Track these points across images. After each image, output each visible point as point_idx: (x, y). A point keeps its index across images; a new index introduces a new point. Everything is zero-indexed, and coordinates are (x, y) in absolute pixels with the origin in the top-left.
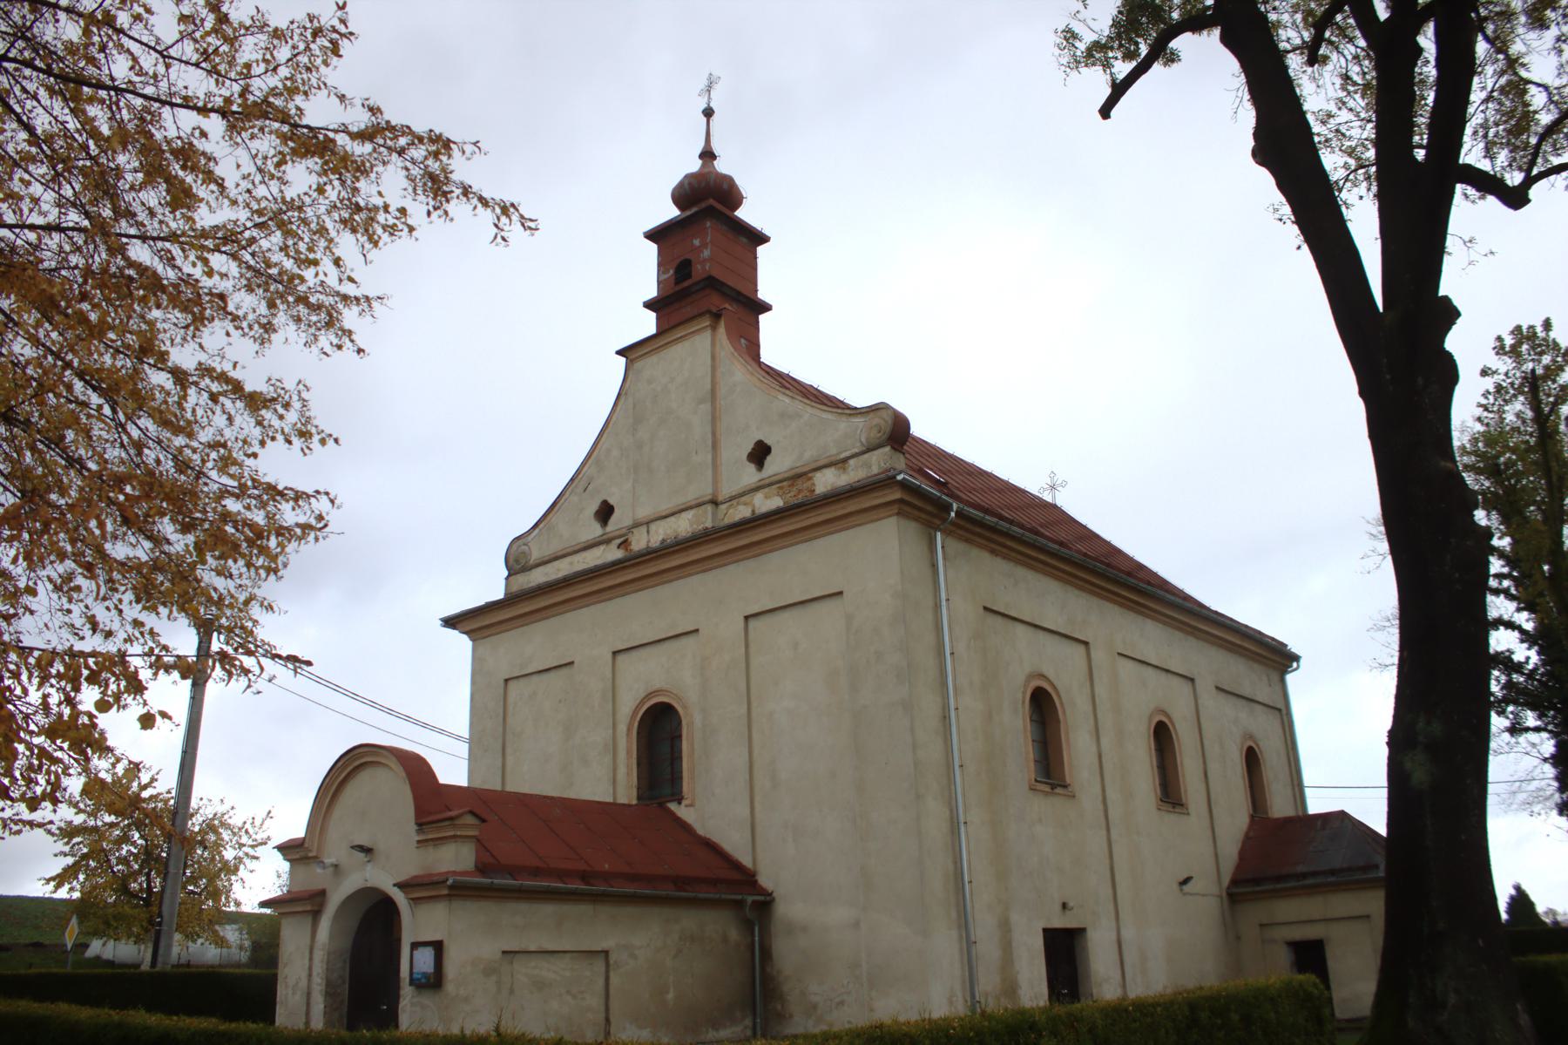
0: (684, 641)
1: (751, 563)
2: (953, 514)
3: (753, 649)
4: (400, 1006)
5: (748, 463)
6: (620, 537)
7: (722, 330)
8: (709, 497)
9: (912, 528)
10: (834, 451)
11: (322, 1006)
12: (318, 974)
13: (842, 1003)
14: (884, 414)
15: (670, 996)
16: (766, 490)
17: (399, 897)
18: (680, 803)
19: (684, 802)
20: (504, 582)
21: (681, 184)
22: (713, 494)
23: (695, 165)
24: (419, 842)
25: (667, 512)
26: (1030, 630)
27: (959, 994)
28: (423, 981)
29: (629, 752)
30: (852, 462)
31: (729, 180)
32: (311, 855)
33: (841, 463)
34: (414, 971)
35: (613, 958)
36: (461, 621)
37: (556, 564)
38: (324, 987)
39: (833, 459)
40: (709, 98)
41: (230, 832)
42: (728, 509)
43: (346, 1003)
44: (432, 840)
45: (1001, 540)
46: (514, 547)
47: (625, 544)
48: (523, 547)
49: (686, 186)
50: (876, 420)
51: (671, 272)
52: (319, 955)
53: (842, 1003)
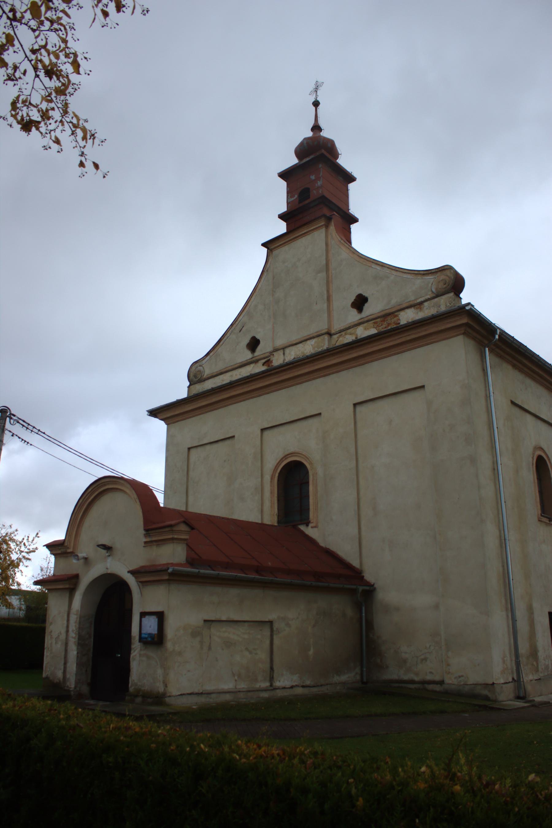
0: (311, 421)
1: (358, 370)
2: (497, 337)
3: (359, 425)
4: (132, 656)
5: (352, 309)
6: (264, 358)
7: (332, 228)
8: (326, 331)
9: (471, 345)
10: (412, 298)
11: (75, 653)
12: (73, 631)
13: (425, 659)
14: (448, 272)
15: (311, 652)
16: (365, 324)
17: (131, 580)
18: (307, 525)
19: (310, 525)
20: (187, 389)
21: (301, 144)
22: (328, 329)
23: (310, 134)
24: (145, 543)
25: (297, 341)
26: (533, 419)
27: (508, 656)
28: (149, 639)
29: (272, 493)
30: (426, 304)
31: (332, 143)
32: (69, 551)
33: (418, 305)
34: (143, 632)
35: (276, 626)
36: (159, 413)
37: (221, 377)
38: (77, 639)
39: (411, 303)
40: (317, 95)
41: (15, 544)
42: (338, 338)
43: (92, 650)
44: (156, 541)
45: (520, 358)
46: (194, 368)
47: (268, 362)
48: (199, 368)
49: (305, 144)
50: (442, 277)
51: (296, 196)
52: (74, 618)
53: (425, 659)
